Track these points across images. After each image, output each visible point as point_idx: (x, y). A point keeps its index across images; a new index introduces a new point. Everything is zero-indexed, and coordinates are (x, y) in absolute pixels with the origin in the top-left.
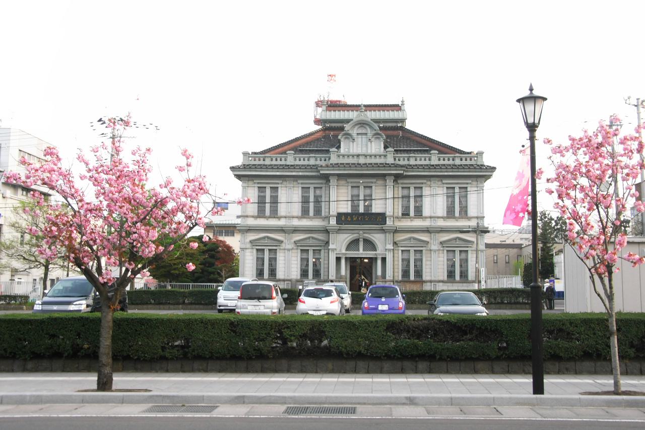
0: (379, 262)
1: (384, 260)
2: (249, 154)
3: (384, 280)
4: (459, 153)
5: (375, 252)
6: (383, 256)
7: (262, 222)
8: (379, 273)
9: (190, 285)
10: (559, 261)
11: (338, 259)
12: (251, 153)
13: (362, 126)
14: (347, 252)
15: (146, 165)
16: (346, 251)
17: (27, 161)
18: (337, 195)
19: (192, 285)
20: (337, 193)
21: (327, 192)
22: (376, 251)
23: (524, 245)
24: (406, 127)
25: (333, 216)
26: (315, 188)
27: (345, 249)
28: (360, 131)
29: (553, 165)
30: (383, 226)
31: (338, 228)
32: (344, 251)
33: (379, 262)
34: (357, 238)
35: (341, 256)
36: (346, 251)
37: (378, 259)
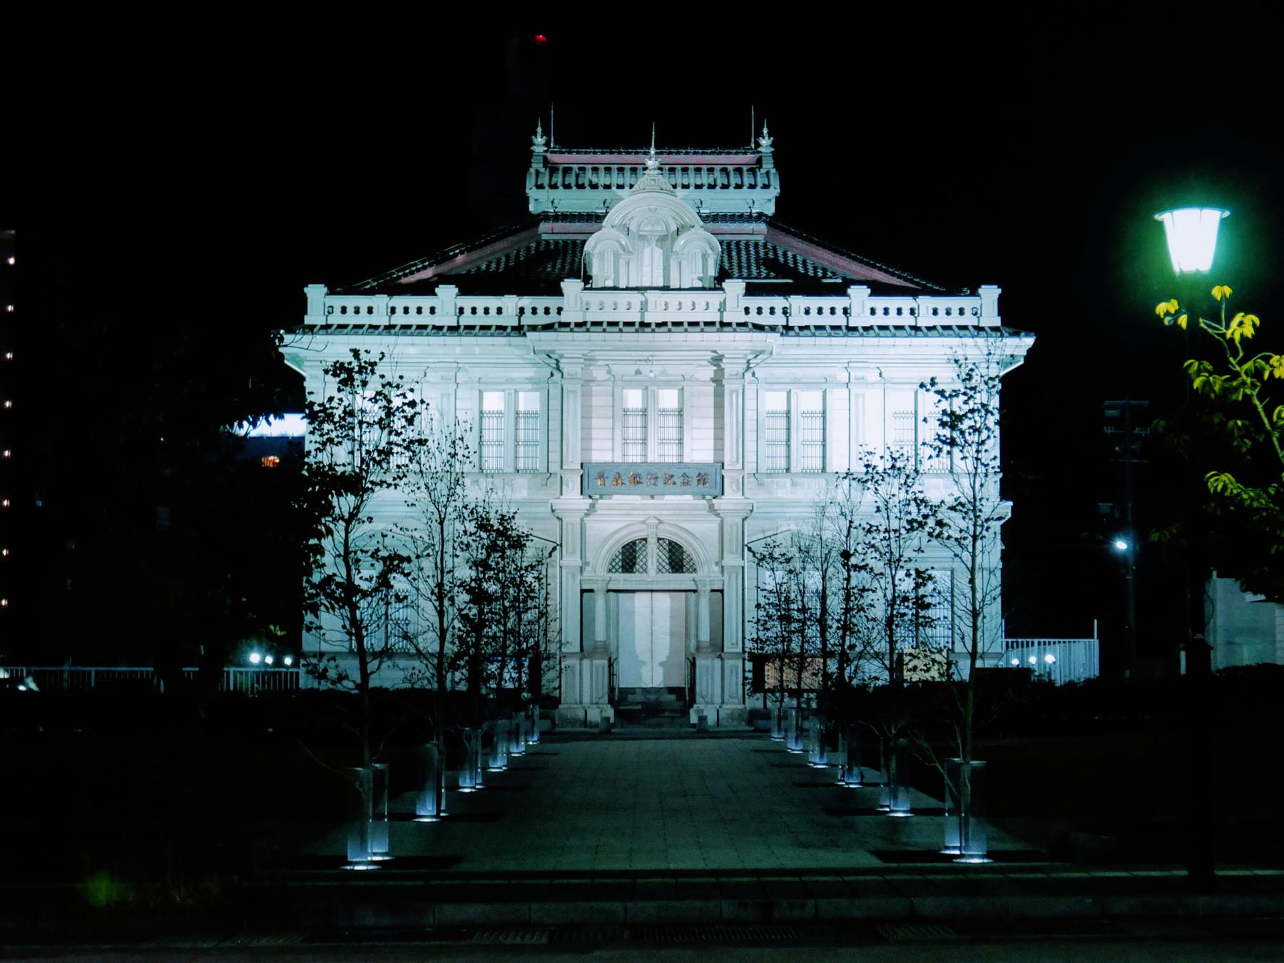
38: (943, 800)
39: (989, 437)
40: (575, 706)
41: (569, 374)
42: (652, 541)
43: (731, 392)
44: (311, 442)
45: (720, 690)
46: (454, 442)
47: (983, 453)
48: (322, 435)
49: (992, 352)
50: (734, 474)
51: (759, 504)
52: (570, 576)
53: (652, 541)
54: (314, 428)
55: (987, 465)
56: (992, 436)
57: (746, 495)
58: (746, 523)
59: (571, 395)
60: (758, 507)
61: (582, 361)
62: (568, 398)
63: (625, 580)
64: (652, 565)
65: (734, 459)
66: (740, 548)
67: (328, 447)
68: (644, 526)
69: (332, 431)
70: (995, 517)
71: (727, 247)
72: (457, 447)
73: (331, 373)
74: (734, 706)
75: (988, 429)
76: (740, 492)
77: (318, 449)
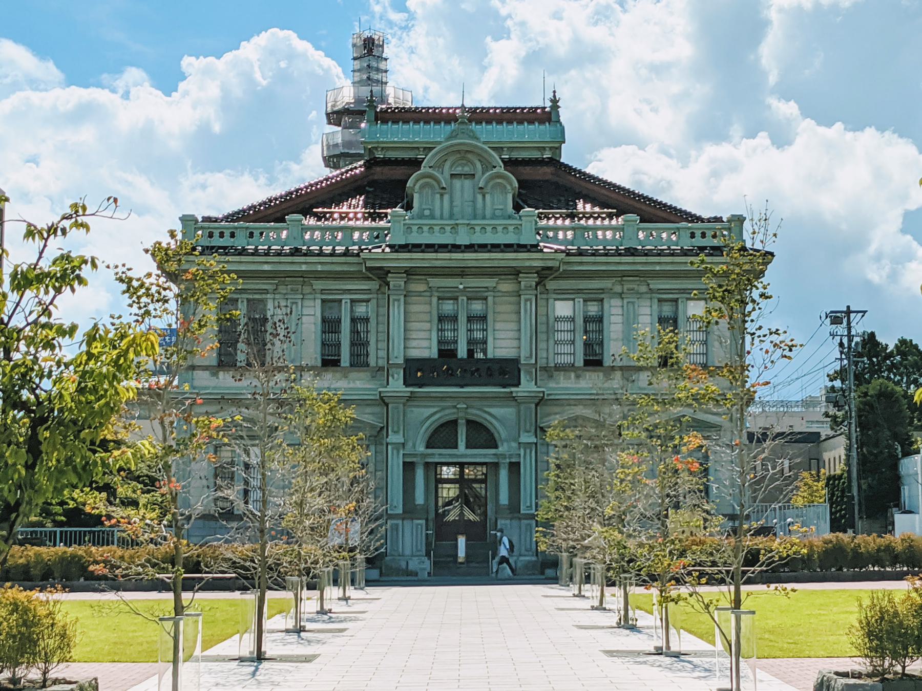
0: (504, 474)
1: (515, 468)
2: (196, 221)
3: (516, 515)
4: (687, 220)
5: (493, 451)
6: (513, 460)
7: (226, 381)
8: (504, 499)
9: (55, 532)
10: (911, 472)
11: (409, 467)
12: (200, 219)
13: (463, 158)
14: (430, 451)
15: (717, 679)
16: (427, 447)
17: (710, 608)
18: (405, 335)
19: (61, 532)
20: (405, 303)
21: (383, 311)
22: (496, 447)
23: (823, 437)
24: (562, 160)
25: (397, 366)
26: (353, 301)
27: (424, 444)
28: (459, 170)
29: (169, 625)
30: (513, 389)
31: (408, 394)
32: (421, 449)
33: (504, 474)
34: (453, 417)
35: (414, 460)
36: (427, 447)
37: (502, 466)
38: (713, 643)
39: (754, 309)
40: (398, 558)
41: (394, 286)
42: (462, 422)
43: (526, 300)
44: (131, 314)
45: (406, 535)
46: (275, 323)
47: (749, 323)
48: (140, 308)
49: (757, 231)
50: (528, 368)
51: (549, 392)
52: (395, 452)
53: (462, 422)
54: (134, 302)
55: (754, 334)
56: (757, 308)
57: (538, 384)
58: (538, 408)
59: (396, 303)
60: (548, 395)
61: (405, 275)
62: (394, 305)
63: (440, 454)
64: (462, 441)
65: (528, 355)
66: (533, 428)
67: (147, 320)
68: (455, 410)
69: (149, 304)
70: (761, 382)
71: (522, 183)
72: (278, 329)
73: (150, 252)
74: (527, 558)
75: (753, 301)
76: (534, 382)
77: (137, 321)
